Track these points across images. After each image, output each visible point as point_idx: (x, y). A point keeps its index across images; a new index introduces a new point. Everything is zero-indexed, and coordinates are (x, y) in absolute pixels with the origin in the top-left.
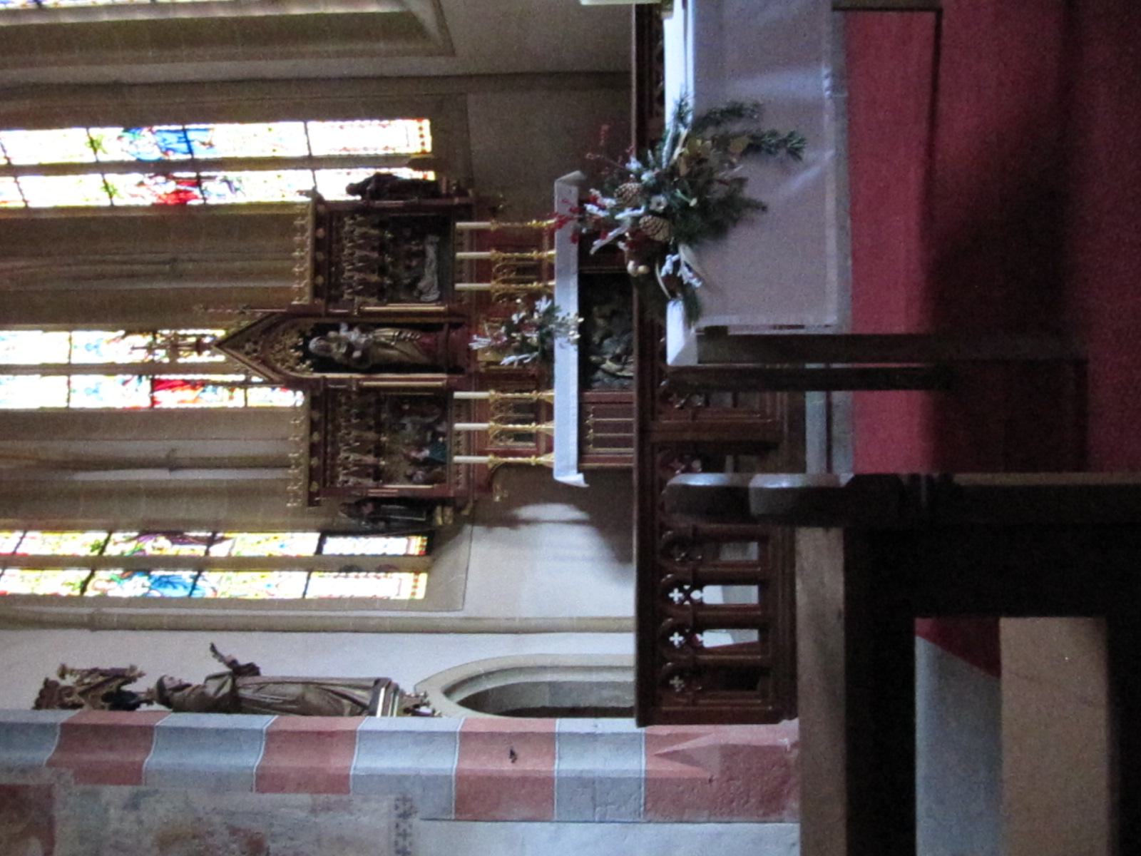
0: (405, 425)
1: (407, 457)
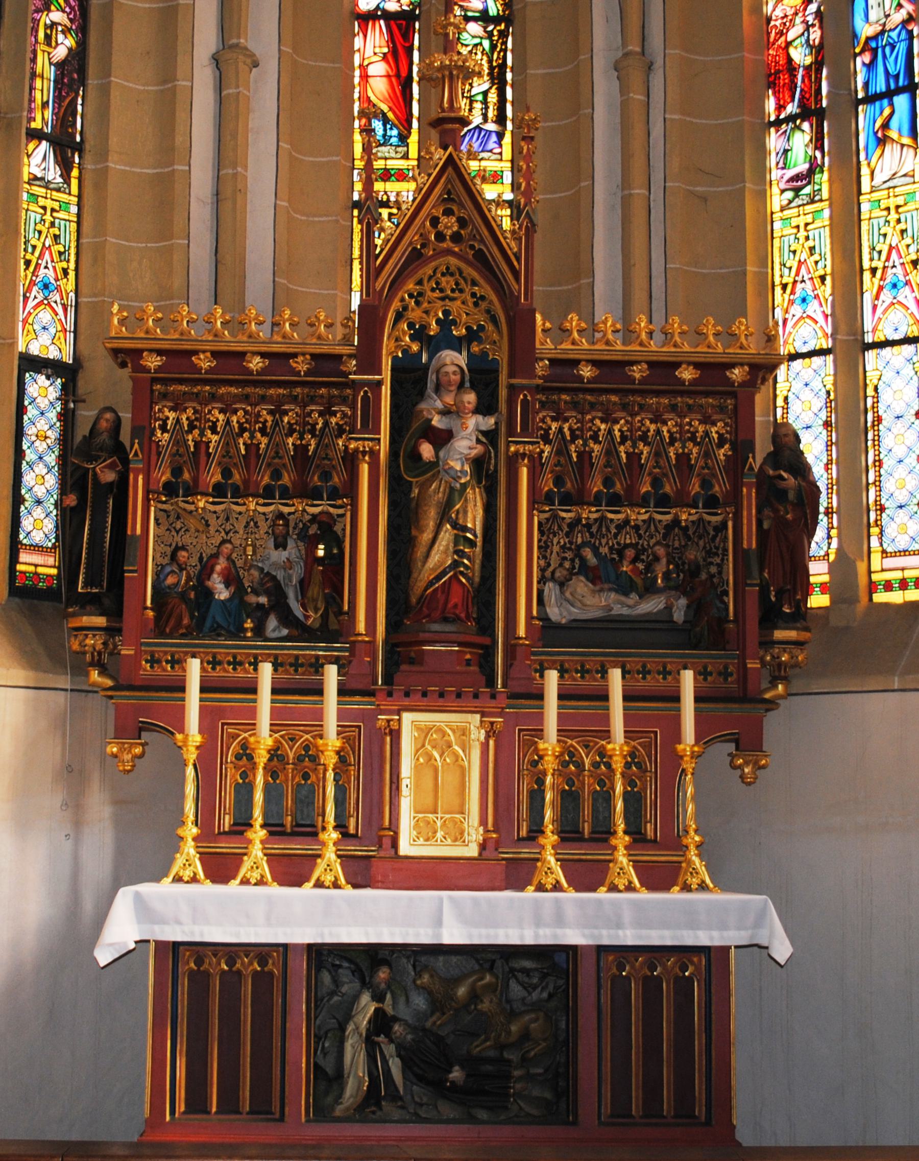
0: (285, 548)
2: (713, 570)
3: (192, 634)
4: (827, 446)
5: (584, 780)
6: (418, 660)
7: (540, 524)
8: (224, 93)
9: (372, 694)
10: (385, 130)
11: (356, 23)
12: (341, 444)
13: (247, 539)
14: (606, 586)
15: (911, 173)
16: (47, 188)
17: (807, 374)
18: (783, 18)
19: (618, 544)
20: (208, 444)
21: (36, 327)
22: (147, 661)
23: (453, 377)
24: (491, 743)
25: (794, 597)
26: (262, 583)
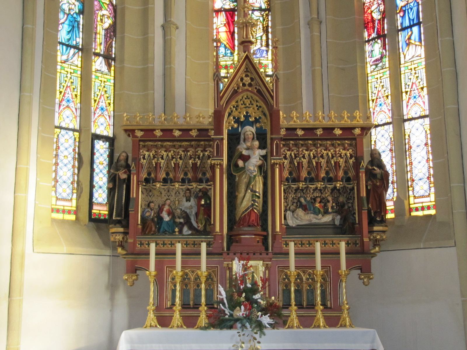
0: (190, 201)
2: (350, 205)
3: (156, 234)
4: (391, 158)
5: (303, 285)
6: (238, 241)
7: (284, 190)
8: (166, 38)
9: (221, 254)
10: (225, 51)
11: (214, 13)
12: (209, 162)
13: (176, 198)
14: (309, 212)
15: (420, 55)
16: (102, 74)
17: (383, 132)
18: (369, 2)
19: (314, 196)
20: (160, 163)
21: (99, 124)
22: (139, 244)
23: (250, 136)
24: (267, 272)
25: (381, 214)
26: (181, 214)
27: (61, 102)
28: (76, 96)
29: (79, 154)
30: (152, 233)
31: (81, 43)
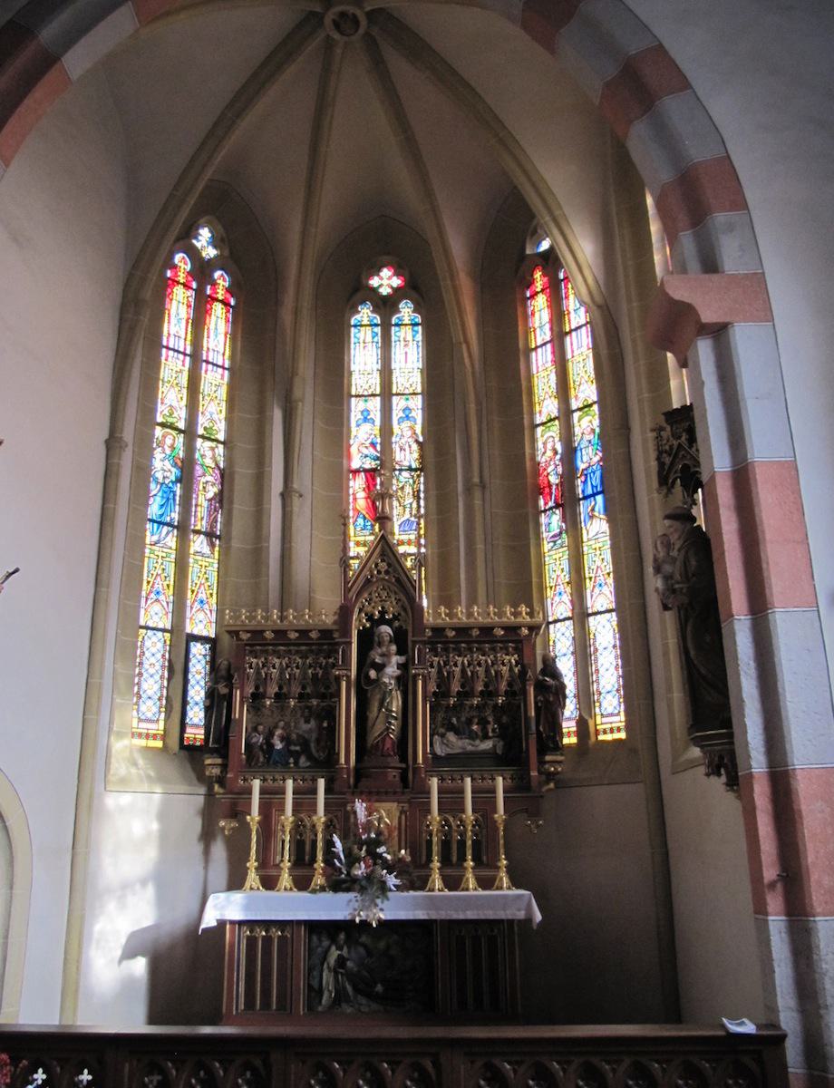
1: (276, 727)
21: (197, 621)
27: (149, 594)
28: (168, 586)
29: (170, 661)
30: (259, 764)
31: (177, 519)
